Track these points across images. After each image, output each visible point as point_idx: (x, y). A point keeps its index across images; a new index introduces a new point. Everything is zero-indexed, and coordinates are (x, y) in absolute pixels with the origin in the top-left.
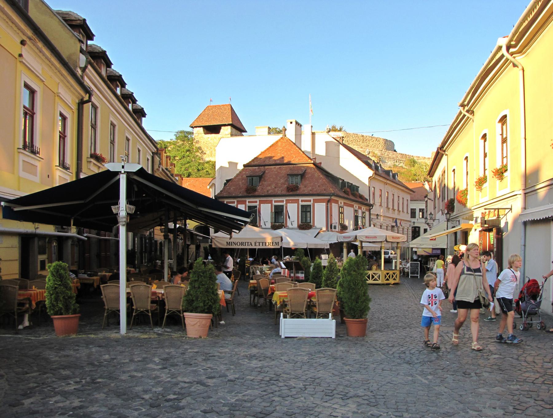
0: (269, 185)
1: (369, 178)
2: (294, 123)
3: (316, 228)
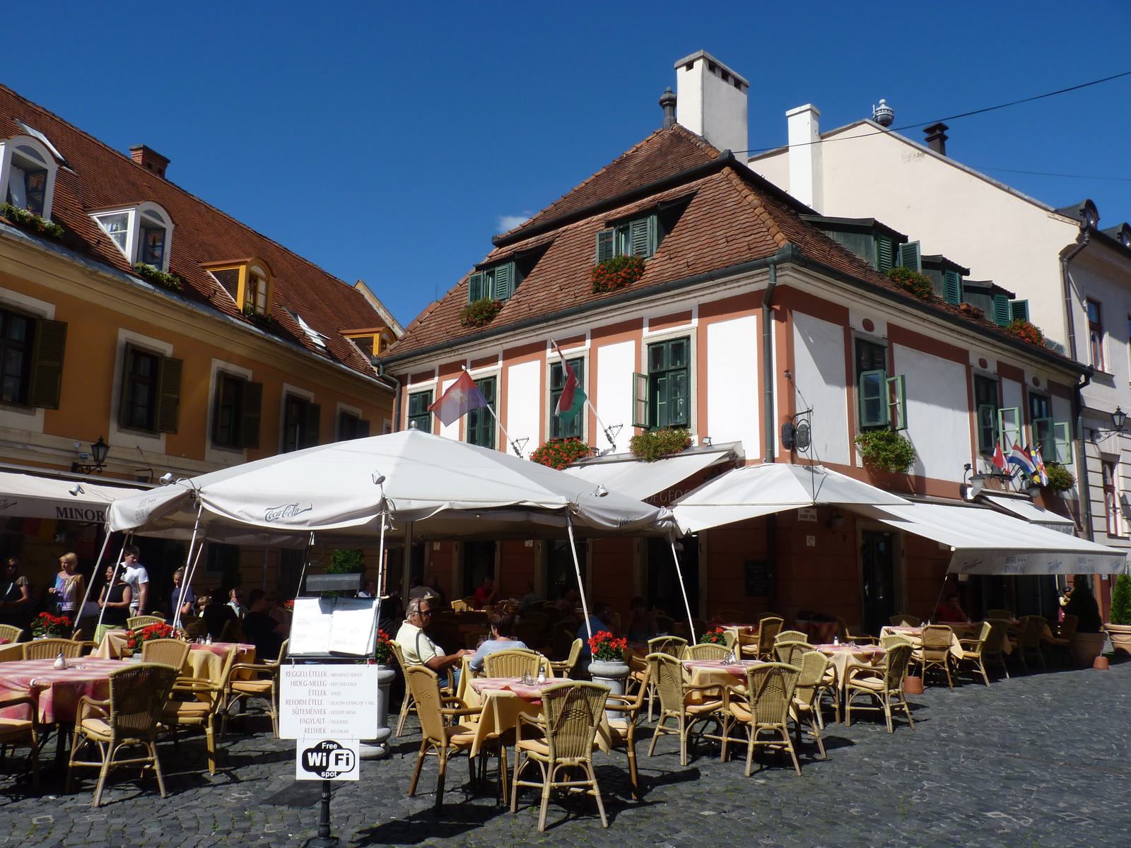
0: (546, 286)
1: (1060, 254)
2: (699, 65)
3: (708, 448)
